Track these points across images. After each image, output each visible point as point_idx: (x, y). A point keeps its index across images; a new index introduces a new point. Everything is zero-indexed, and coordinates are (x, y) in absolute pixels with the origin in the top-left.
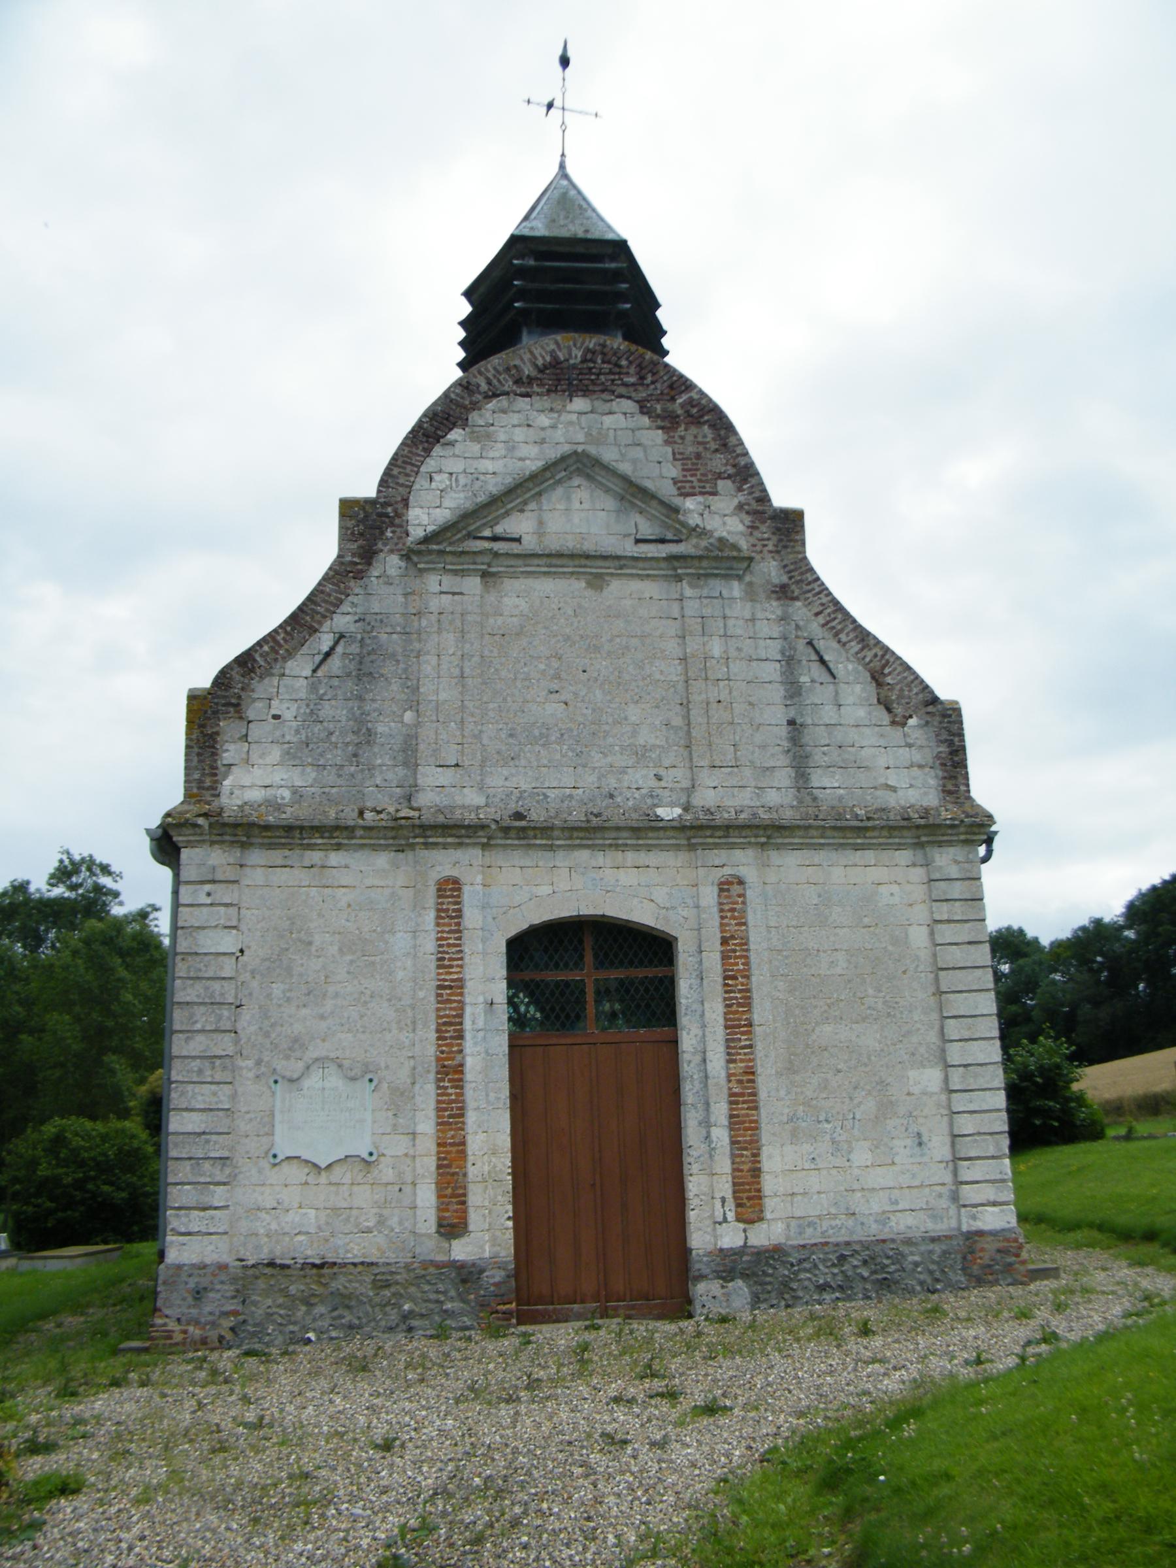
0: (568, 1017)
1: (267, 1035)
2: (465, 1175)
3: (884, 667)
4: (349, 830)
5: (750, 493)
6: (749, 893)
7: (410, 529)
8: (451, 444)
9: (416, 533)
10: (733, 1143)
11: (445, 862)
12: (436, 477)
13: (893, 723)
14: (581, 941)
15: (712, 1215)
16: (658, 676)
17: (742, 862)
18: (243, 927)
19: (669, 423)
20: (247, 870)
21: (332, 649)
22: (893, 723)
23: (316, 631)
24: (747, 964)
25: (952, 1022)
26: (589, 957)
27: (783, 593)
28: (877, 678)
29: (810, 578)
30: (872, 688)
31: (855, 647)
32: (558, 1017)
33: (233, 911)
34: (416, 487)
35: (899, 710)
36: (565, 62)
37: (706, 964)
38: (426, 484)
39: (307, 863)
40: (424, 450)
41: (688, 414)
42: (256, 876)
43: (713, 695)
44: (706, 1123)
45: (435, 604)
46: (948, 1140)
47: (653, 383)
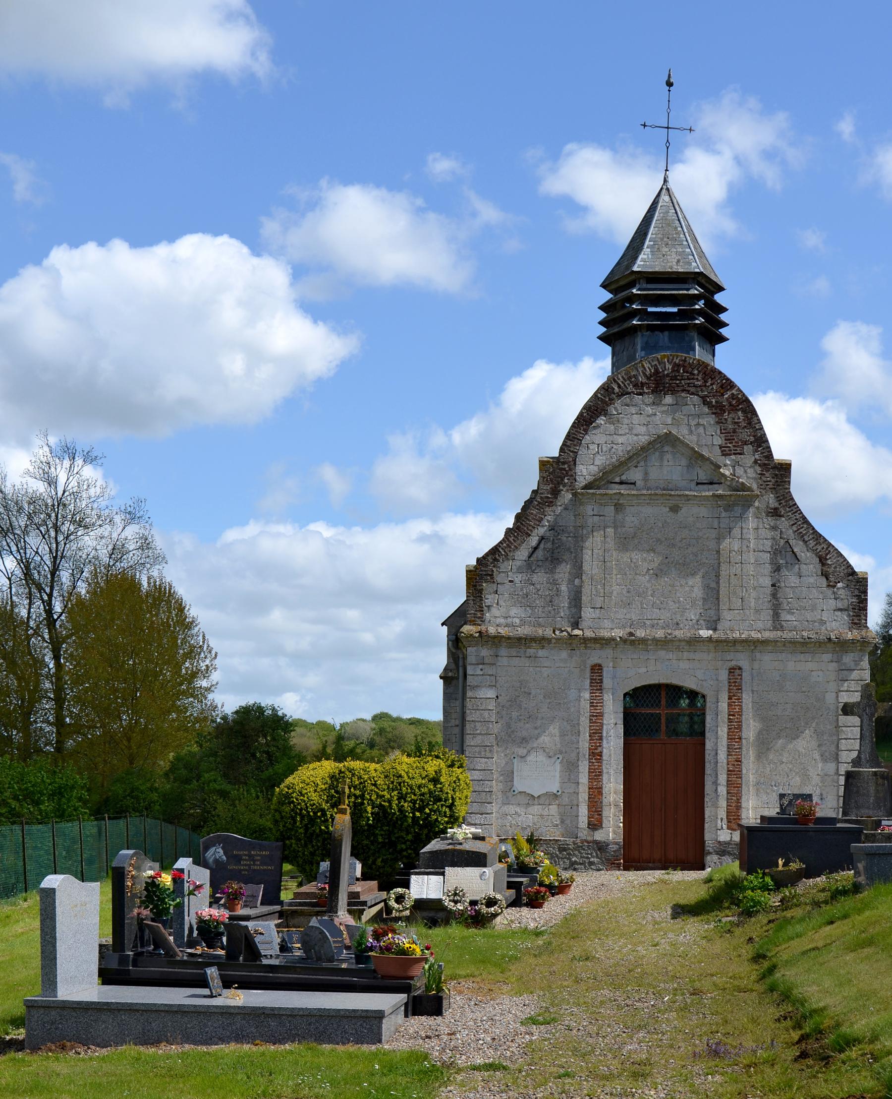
0: (652, 730)
1: (510, 736)
2: (601, 802)
3: (827, 555)
4: (549, 641)
5: (762, 453)
6: (744, 674)
7: (577, 478)
8: (598, 427)
9: (581, 482)
10: (728, 793)
11: (595, 657)
12: (591, 447)
13: (829, 586)
14: (660, 694)
15: (716, 826)
16: (704, 560)
17: (742, 660)
18: (498, 685)
19: (718, 410)
20: (499, 658)
21: (538, 545)
22: (829, 586)
23: (530, 535)
24: (741, 709)
25: (843, 741)
26: (663, 702)
27: (775, 513)
28: (822, 561)
29: (791, 503)
30: (819, 566)
31: (812, 543)
32: (647, 730)
33: (493, 678)
34: (580, 452)
35: (832, 579)
36: (670, 84)
37: (720, 708)
38: (586, 452)
39: (528, 655)
40: (584, 430)
41: (730, 404)
42: (503, 661)
43: (733, 571)
44: (716, 783)
45: (590, 522)
46: (836, 798)
47: (712, 384)
